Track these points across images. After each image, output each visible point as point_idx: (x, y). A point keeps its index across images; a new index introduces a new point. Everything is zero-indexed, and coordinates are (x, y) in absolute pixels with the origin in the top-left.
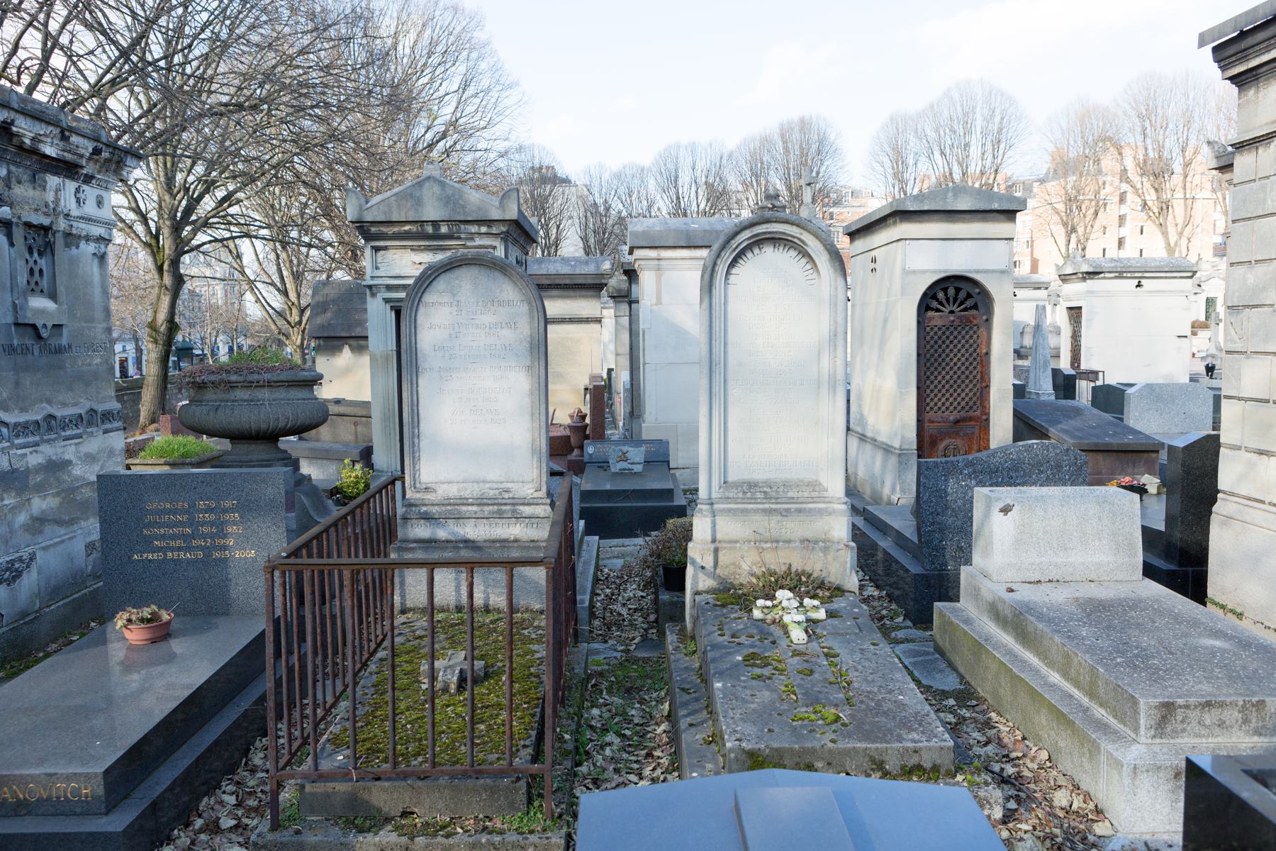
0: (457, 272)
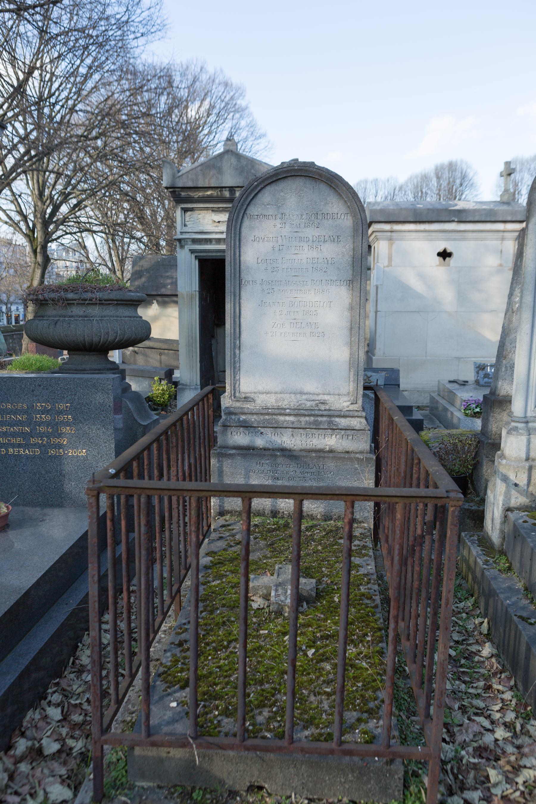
0: (282, 185)
